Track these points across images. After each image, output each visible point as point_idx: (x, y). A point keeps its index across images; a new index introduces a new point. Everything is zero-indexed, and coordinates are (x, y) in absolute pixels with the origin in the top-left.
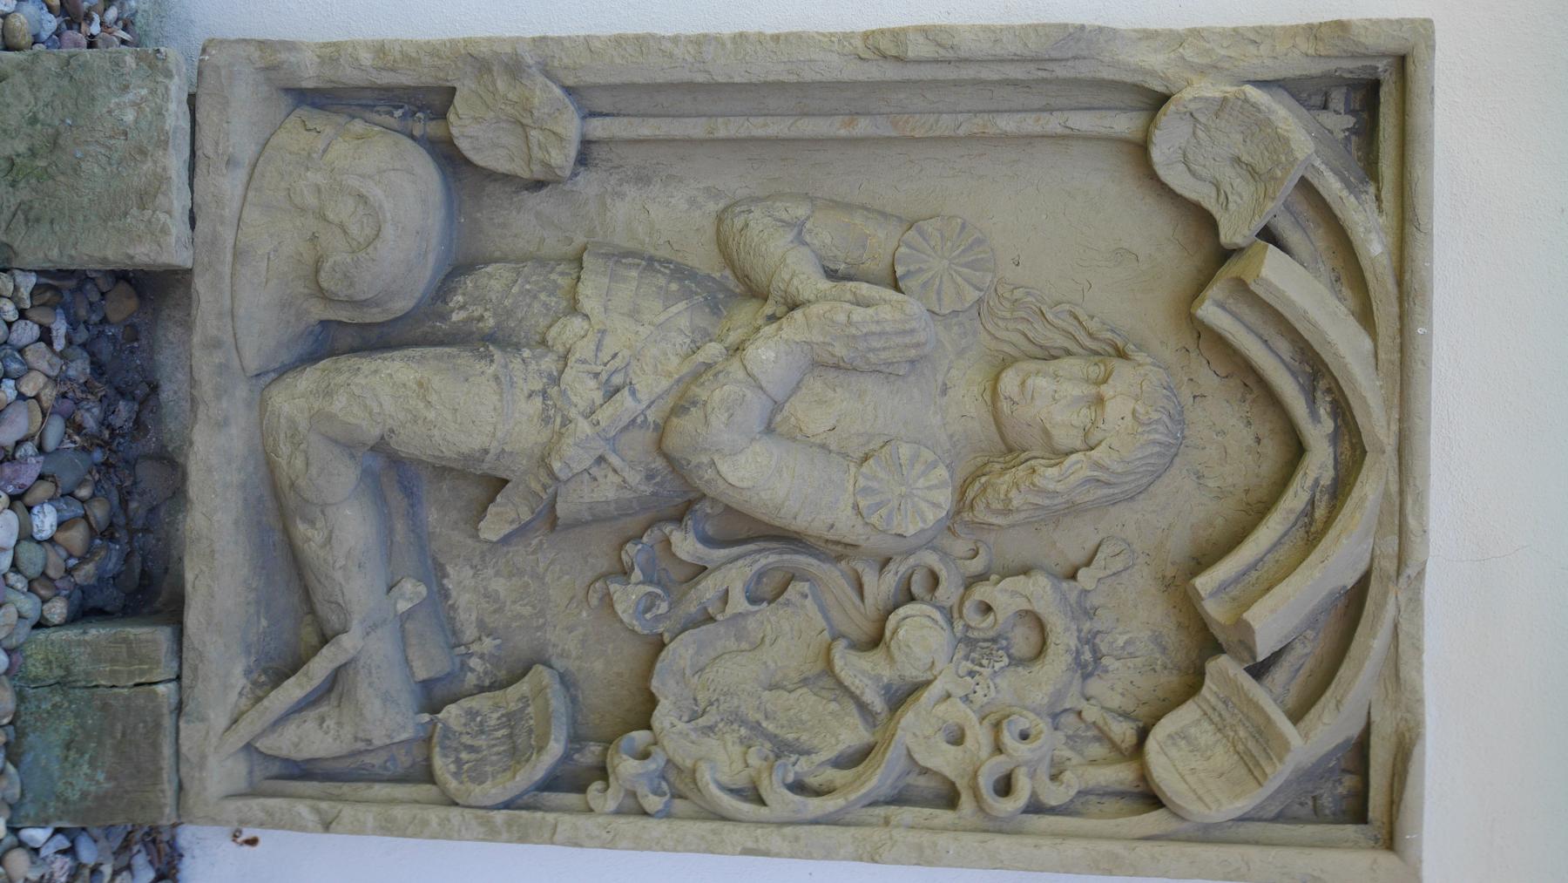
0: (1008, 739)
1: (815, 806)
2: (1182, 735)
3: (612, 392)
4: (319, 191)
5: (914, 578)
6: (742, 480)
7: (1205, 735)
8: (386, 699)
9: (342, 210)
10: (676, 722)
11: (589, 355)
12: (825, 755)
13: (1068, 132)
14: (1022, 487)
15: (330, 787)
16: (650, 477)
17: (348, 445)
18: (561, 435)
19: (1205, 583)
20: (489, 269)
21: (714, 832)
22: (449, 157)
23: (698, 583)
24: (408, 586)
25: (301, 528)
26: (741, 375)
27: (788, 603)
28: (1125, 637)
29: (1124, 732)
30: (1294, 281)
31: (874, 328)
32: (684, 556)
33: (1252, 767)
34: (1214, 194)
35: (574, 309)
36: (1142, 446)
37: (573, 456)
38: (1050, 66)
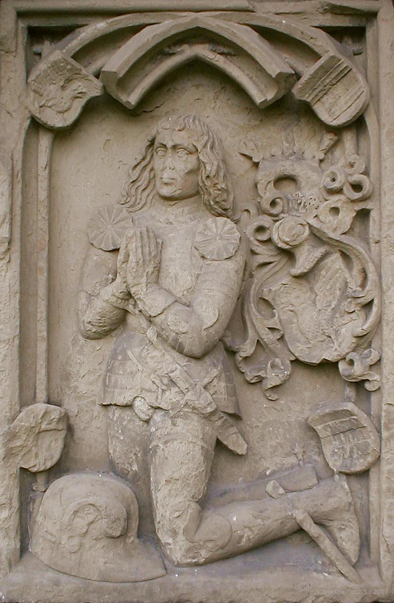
0: (336, 185)
1: (372, 276)
2: (329, 111)
3: (172, 382)
4: (72, 537)
5: (258, 239)
6: (215, 314)
7: (328, 100)
8: (329, 495)
9: (81, 523)
10: (334, 348)
11: (154, 395)
12: (347, 275)
13: (48, 168)
14: (216, 182)
15: (372, 525)
16: (215, 366)
17: (199, 519)
18: (194, 408)
19: (258, 98)
20: (111, 451)
21: (388, 324)
22: (56, 471)
23: (265, 343)
24: (269, 488)
25: (244, 543)
26: (162, 317)
27: (274, 299)
28: (284, 142)
29: (328, 139)
30: (117, 61)
31: (140, 251)
32: (253, 349)
33: (345, 74)
34: (79, 99)
35: (129, 406)
36: (196, 126)
37: (204, 401)
38: (16, 173)
